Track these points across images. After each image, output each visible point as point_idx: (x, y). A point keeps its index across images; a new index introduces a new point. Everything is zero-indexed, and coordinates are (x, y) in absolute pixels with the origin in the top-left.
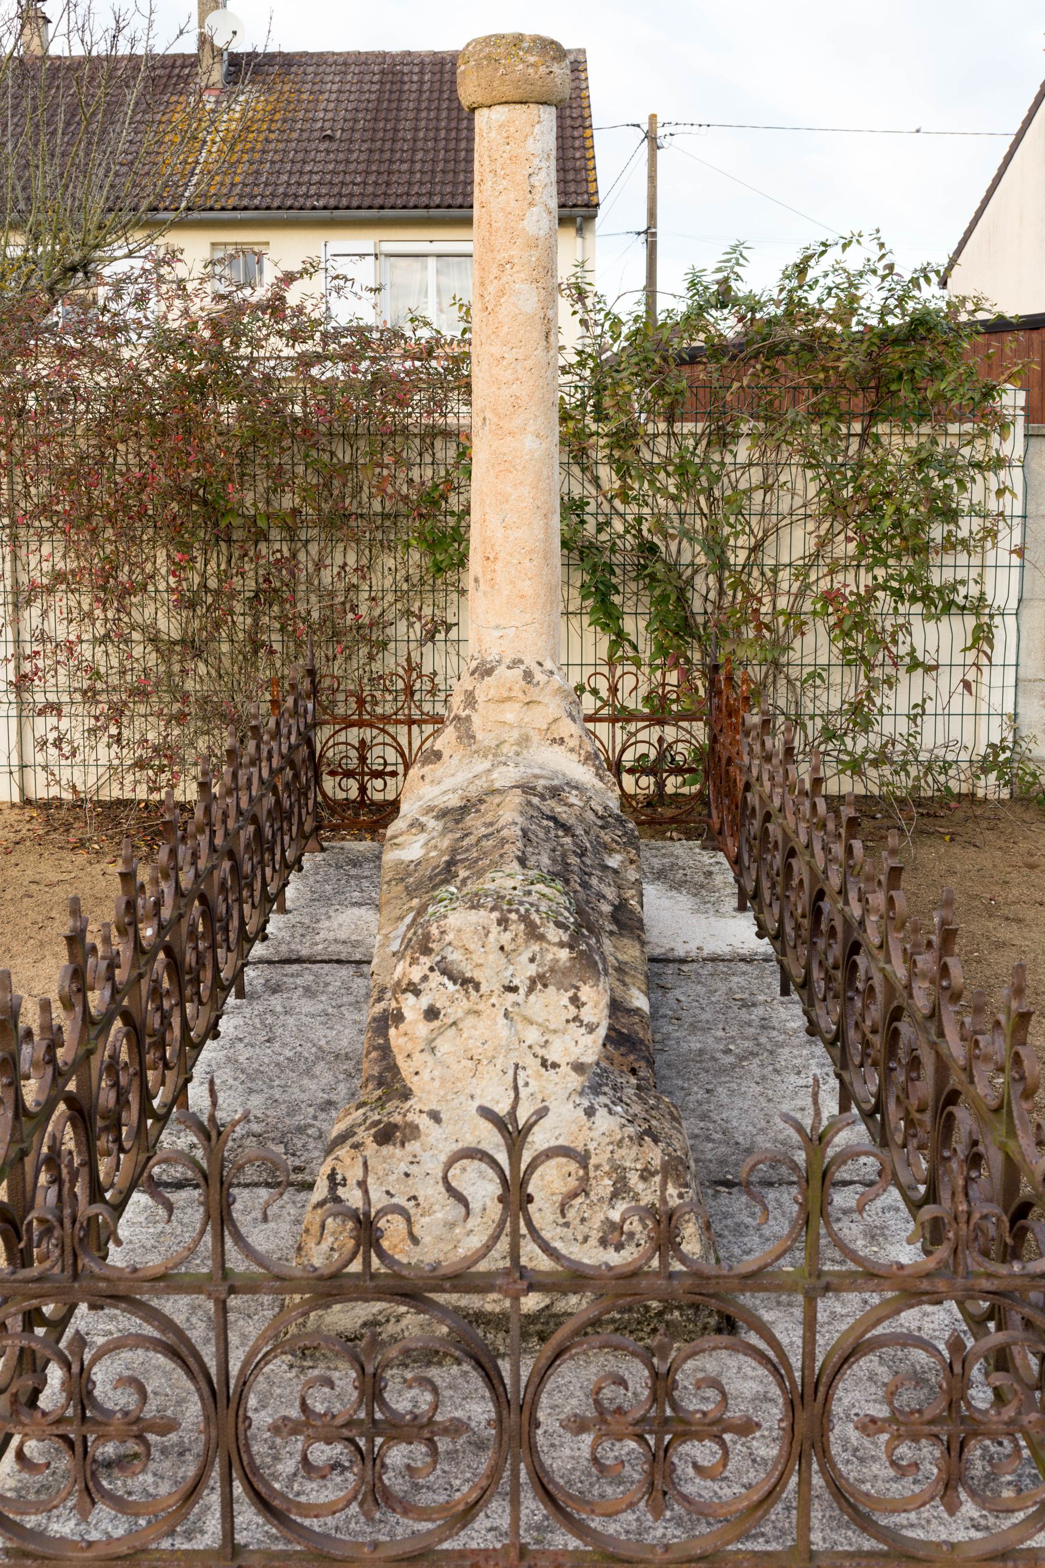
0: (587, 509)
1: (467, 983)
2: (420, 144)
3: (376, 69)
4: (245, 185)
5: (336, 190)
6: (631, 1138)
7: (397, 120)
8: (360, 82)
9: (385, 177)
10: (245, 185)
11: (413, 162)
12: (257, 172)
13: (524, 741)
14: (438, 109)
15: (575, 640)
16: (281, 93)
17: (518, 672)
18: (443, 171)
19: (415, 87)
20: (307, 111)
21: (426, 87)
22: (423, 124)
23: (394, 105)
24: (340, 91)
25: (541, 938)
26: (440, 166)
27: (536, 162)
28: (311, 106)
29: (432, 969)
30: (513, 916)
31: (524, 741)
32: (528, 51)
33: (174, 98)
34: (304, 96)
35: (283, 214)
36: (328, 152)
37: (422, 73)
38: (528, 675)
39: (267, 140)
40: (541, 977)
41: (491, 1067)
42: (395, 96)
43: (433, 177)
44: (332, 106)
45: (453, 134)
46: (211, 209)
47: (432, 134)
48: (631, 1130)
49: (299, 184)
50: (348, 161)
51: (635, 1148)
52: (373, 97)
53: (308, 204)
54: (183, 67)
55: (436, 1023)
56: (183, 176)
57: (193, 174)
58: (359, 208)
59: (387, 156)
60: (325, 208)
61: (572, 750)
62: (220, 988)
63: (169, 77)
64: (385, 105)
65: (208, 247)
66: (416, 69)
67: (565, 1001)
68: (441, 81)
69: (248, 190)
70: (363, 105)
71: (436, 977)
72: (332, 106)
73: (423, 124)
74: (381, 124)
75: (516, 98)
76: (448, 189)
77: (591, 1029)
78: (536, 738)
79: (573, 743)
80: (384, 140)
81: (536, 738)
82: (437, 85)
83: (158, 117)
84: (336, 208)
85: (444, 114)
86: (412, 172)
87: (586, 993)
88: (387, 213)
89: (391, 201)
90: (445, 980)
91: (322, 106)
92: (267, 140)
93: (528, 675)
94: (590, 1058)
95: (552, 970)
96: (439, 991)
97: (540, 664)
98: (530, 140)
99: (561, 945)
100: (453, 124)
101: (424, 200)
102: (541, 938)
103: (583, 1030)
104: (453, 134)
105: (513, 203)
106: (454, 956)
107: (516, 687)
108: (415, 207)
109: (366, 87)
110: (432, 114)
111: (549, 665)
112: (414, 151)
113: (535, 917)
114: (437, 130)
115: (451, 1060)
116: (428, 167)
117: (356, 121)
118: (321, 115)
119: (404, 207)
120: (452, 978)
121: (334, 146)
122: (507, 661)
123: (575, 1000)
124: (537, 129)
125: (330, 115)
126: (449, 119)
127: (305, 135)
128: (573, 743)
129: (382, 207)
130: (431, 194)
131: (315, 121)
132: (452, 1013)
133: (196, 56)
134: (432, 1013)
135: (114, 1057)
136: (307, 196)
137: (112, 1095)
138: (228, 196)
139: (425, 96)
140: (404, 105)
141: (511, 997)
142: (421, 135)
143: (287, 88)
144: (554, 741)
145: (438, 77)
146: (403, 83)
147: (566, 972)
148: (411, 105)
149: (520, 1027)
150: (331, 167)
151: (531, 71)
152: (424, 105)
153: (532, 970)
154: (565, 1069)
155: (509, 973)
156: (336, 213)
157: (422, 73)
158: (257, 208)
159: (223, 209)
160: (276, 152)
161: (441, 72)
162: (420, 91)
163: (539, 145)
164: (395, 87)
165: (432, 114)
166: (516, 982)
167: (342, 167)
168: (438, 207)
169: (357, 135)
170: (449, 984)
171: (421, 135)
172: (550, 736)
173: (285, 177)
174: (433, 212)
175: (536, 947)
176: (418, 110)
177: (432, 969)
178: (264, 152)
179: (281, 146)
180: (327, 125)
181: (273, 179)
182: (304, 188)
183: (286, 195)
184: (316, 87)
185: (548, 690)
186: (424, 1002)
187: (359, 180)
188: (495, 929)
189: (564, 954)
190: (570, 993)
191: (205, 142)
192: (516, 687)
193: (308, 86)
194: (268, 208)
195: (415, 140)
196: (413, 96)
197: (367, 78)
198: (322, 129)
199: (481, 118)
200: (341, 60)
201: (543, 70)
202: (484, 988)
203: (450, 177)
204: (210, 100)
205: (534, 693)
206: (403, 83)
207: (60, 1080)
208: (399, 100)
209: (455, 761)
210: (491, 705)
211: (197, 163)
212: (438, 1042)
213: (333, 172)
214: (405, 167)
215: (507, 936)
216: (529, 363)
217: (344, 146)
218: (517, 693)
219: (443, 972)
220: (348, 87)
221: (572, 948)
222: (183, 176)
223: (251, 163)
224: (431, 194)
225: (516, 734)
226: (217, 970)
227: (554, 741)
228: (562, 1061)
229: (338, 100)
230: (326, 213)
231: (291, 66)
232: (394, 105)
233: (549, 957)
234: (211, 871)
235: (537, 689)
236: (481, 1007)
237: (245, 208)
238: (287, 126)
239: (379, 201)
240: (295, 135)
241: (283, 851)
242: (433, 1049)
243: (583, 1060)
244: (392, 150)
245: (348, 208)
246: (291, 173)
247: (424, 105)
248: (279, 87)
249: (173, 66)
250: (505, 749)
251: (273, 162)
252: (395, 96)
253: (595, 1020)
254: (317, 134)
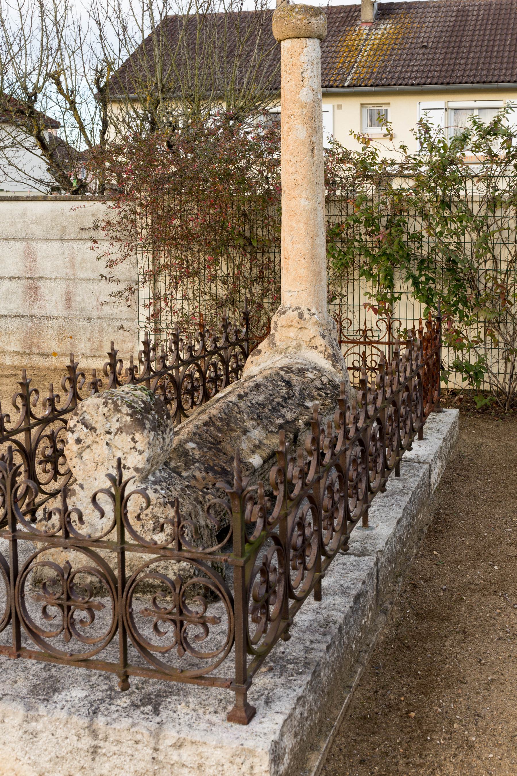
0: (423, 239)
1: (92, 429)
2: (473, 49)
3: (455, 9)
4: (379, 73)
5: (425, 75)
6: (160, 503)
7: (462, 36)
8: (445, 16)
9: (452, 67)
10: (379, 73)
11: (468, 58)
12: (386, 66)
13: (299, 347)
14: (485, 30)
15: (410, 306)
16: (403, 24)
17: (296, 313)
18: (483, 63)
19: (474, 18)
20: (415, 33)
21: (480, 18)
22: (476, 38)
23: (462, 28)
24: (434, 22)
25: (119, 411)
26: (482, 60)
27: (305, 66)
28: (418, 30)
29: (78, 422)
30: (110, 401)
31: (299, 347)
32: (297, 13)
33: (348, 28)
34: (415, 25)
35: (397, 88)
36: (424, 54)
37: (479, 10)
38: (301, 315)
39: (393, 49)
40: (121, 428)
41: (102, 467)
42: (463, 23)
43: (477, 67)
44: (429, 29)
45: (491, 43)
46: (360, 86)
47: (480, 43)
48: (162, 500)
49: (406, 72)
50: (433, 59)
51: (162, 508)
52: (451, 24)
53: (410, 82)
54: (355, 12)
55: (80, 446)
56: (348, 69)
57: (353, 68)
58: (436, 84)
59: (454, 55)
60: (418, 84)
61: (321, 352)
62: (370, 492)
63: (347, 17)
64: (457, 28)
65: (359, 106)
66: (476, 8)
67: (130, 440)
68: (488, 14)
69: (379, 75)
70: (445, 29)
71: (80, 426)
72: (429, 29)
73: (476, 38)
74: (454, 39)
75: (293, 36)
76: (485, 73)
77: (141, 453)
78: (304, 345)
79: (321, 349)
80: (454, 47)
81: (304, 345)
82: (486, 17)
83: (339, 38)
84: (424, 84)
85: (488, 32)
86: (466, 64)
87: (138, 436)
88: (451, 86)
89: (453, 80)
90: (83, 427)
91: (424, 30)
92: (393, 49)
93: (301, 315)
94: (140, 466)
95: (125, 426)
96: (81, 431)
97: (309, 310)
98: (302, 55)
99: (127, 415)
100: (492, 37)
101: (471, 79)
102: (119, 411)
103: (137, 453)
104: (491, 43)
105: (294, 87)
106: (88, 417)
107: (295, 320)
108: (466, 83)
109: (448, 19)
110: (482, 32)
111: (313, 310)
112: (469, 52)
113: (119, 402)
114: (483, 41)
115: (88, 462)
116: (476, 61)
117: (440, 37)
118: (423, 34)
119: (460, 83)
120: (87, 427)
121: (427, 51)
122: (293, 308)
123: (133, 439)
124: (305, 50)
125: (427, 35)
126: (490, 35)
127: (413, 46)
128: (321, 349)
129: (448, 83)
130: (475, 76)
131: (419, 38)
132: (88, 441)
133: (360, 6)
134: (78, 441)
135: (302, 519)
136: (410, 78)
137: (300, 539)
138: (369, 79)
139: (479, 23)
140: (467, 28)
141: (108, 436)
142: (474, 44)
143: (407, 21)
144: (313, 347)
145: (487, 12)
146: (468, 16)
147: (130, 427)
148: (471, 28)
149: (114, 450)
150: (424, 62)
151: (299, 22)
152: (478, 27)
153: (118, 425)
154: (132, 470)
155: (108, 426)
156: (424, 87)
157: (479, 10)
158: (383, 85)
159: (366, 86)
160: (397, 55)
161: (490, 10)
162: (477, 20)
163: (306, 58)
164: (464, 18)
165: (482, 32)
166: (112, 430)
167: (430, 62)
168: (478, 82)
169: (440, 45)
170: (85, 429)
171: (474, 44)
172: (311, 345)
173: (400, 69)
174: (476, 85)
175: (119, 415)
176: (474, 30)
177: (78, 422)
178: (390, 55)
179: (400, 52)
180: (425, 40)
181: (393, 69)
182: (409, 74)
183: (399, 78)
184: (422, 20)
185: (311, 322)
186: (76, 436)
187: (438, 69)
188: (101, 406)
189: (128, 418)
190: (131, 436)
191: (361, 51)
192: (295, 320)
193: (418, 20)
194: (389, 85)
195: (470, 47)
196: (473, 23)
197: (450, 14)
198: (422, 42)
199: (285, 45)
200: (437, 5)
201: (305, 22)
202: (98, 432)
203: (487, 66)
204: (365, 29)
205: (303, 323)
206: (468, 16)
207: (268, 527)
208: (465, 25)
209: (267, 355)
210: (284, 329)
211: (356, 62)
212: (83, 455)
213: (425, 65)
214: (463, 61)
215: (106, 409)
216: (302, 164)
217: (433, 51)
218: (295, 323)
219: (83, 424)
220: (438, 19)
221: (131, 416)
222: (348, 69)
223: (383, 61)
224: (475, 76)
225: (295, 343)
226: (368, 482)
227: (313, 347)
228: (131, 466)
229: (432, 27)
230: (419, 87)
231: (410, 9)
232: (462, 28)
233: (124, 420)
234: (365, 429)
235: (305, 322)
236: (97, 440)
237: (377, 85)
238: (404, 41)
239: (447, 80)
240: (408, 46)
241: (412, 423)
242: (81, 458)
243: (138, 466)
244: (458, 53)
245: (430, 84)
246: (403, 66)
247: (478, 27)
248: (402, 20)
249: (350, 11)
250: (290, 350)
251: (394, 61)
252: (463, 23)
253: (142, 449)
254: (419, 45)
